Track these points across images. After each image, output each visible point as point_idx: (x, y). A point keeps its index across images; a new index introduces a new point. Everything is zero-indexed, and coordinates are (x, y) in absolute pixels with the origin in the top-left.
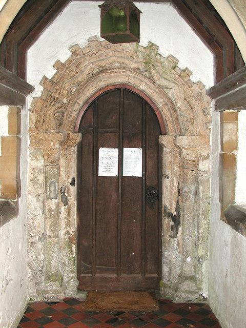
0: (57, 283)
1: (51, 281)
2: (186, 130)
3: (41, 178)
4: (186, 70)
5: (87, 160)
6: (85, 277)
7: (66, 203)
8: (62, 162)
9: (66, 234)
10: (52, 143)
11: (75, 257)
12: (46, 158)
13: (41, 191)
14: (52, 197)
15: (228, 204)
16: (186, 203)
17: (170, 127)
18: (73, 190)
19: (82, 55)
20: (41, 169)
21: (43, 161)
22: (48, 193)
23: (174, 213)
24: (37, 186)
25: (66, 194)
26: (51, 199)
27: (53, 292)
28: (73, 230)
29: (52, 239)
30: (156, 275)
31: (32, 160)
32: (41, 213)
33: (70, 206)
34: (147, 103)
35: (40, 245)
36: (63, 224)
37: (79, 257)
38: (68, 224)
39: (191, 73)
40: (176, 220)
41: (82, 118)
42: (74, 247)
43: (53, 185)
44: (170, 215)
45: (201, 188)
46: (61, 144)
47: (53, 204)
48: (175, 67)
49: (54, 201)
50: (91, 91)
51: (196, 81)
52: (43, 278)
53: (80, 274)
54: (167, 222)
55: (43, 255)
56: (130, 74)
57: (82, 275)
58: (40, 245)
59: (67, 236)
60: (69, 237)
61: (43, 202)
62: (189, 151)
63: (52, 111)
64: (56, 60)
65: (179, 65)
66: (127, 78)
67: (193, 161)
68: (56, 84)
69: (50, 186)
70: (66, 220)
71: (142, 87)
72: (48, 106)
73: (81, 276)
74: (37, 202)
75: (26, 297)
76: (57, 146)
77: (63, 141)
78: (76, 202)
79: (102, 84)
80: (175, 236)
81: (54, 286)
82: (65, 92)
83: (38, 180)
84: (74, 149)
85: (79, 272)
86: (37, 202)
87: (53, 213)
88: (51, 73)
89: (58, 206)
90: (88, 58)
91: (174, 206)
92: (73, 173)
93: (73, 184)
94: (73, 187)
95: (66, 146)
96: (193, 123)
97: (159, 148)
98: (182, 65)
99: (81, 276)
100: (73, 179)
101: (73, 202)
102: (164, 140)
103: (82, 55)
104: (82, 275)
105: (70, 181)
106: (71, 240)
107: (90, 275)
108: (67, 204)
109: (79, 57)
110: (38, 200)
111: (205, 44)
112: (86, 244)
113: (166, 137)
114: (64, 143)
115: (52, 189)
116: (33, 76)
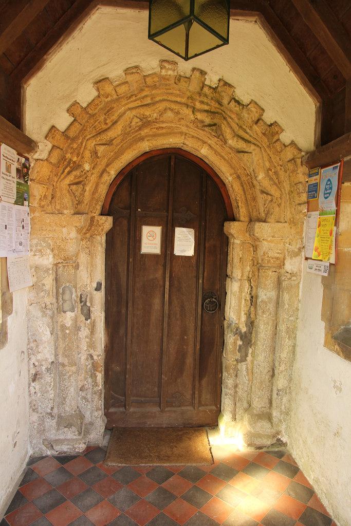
0: (74, 429)
1: (65, 427)
2: (268, 213)
3: (49, 282)
4: (275, 124)
5: (121, 248)
6: (115, 413)
7: (88, 316)
8: (83, 259)
9: (87, 359)
10: (64, 230)
11: (101, 390)
12: (57, 252)
13: (49, 300)
14: (65, 309)
15: (340, 325)
16: (262, 317)
17: (242, 212)
18: (99, 299)
19: (115, 97)
20: (49, 269)
21: (51, 256)
22: (61, 303)
23: (244, 329)
24: (42, 294)
25: (88, 304)
26: (65, 312)
27: (71, 442)
28: (99, 353)
29: (67, 368)
30: (214, 408)
31: (35, 255)
32: (49, 333)
33: (94, 320)
34: (208, 175)
35: (48, 378)
36: (84, 346)
37: (107, 386)
38: (91, 345)
39: (283, 130)
40: (247, 339)
41: (113, 195)
42: (100, 377)
43: (68, 292)
44: (237, 332)
45: (286, 297)
46: (79, 231)
47: (68, 318)
48: (258, 120)
49: (70, 315)
50: (128, 157)
51: (287, 142)
52: (54, 423)
53: (108, 410)
54: (231, 340)
55: (52, 392)
56: (187, 132)
57: (112, 410)
58: (48, 378)
59: (90, 362)
60: (93, 363)
61: (52, 318)
62: (273, 245)
63: (67, 181)
64: (74, 100)
65: (265, 117)
66: (183, 137)
67: (277, 258)
68: (74, 140)
69: (63, 293)
70: (87, 340)
71: (204, 152)
72: (59, 174)
73: (109, 411)
74: (43, 317)
75: (27, 452)
76: (73, 234)
77: (82, 228)
78: (103, 315)
79: (145, 146)
80: (243, 359)
81: (70, 434)
82: (87, 154)
83: (44, 285)
84: (102, 239)
85: (107, 406)
86: (43, 317)
87: (68, 332)
88: (63, 121)
89: (75, 320)
90: (124, 102)
91: (243, 318)
92: (100, 275)
93: (98, 289)
94: (98, 293)
95: (88, 235)
96: (280, 204)
97: (224, 241)
98: (269, 117)
99: (109, 411)
100: (99, 284)
101: (99, 314)
102: (233, 229)
103: (115, 97)
104: (112, 410)
105: (95, 285)
106: (95, 366)
107: (122, 409)
108: (90, 318)
109: (109, 99)
110: (44, 315)
111: (304, 83)
112: (118, 368)
113: (236, 223)
114: (87, 232)
115: (67, 297)
116: (34, 120)
